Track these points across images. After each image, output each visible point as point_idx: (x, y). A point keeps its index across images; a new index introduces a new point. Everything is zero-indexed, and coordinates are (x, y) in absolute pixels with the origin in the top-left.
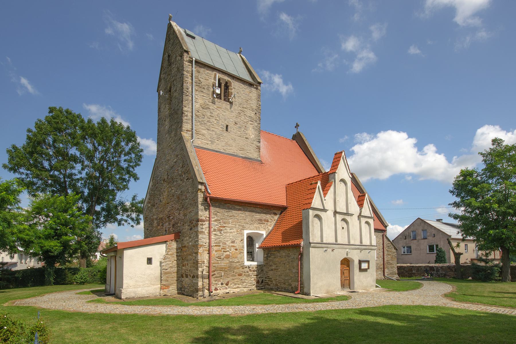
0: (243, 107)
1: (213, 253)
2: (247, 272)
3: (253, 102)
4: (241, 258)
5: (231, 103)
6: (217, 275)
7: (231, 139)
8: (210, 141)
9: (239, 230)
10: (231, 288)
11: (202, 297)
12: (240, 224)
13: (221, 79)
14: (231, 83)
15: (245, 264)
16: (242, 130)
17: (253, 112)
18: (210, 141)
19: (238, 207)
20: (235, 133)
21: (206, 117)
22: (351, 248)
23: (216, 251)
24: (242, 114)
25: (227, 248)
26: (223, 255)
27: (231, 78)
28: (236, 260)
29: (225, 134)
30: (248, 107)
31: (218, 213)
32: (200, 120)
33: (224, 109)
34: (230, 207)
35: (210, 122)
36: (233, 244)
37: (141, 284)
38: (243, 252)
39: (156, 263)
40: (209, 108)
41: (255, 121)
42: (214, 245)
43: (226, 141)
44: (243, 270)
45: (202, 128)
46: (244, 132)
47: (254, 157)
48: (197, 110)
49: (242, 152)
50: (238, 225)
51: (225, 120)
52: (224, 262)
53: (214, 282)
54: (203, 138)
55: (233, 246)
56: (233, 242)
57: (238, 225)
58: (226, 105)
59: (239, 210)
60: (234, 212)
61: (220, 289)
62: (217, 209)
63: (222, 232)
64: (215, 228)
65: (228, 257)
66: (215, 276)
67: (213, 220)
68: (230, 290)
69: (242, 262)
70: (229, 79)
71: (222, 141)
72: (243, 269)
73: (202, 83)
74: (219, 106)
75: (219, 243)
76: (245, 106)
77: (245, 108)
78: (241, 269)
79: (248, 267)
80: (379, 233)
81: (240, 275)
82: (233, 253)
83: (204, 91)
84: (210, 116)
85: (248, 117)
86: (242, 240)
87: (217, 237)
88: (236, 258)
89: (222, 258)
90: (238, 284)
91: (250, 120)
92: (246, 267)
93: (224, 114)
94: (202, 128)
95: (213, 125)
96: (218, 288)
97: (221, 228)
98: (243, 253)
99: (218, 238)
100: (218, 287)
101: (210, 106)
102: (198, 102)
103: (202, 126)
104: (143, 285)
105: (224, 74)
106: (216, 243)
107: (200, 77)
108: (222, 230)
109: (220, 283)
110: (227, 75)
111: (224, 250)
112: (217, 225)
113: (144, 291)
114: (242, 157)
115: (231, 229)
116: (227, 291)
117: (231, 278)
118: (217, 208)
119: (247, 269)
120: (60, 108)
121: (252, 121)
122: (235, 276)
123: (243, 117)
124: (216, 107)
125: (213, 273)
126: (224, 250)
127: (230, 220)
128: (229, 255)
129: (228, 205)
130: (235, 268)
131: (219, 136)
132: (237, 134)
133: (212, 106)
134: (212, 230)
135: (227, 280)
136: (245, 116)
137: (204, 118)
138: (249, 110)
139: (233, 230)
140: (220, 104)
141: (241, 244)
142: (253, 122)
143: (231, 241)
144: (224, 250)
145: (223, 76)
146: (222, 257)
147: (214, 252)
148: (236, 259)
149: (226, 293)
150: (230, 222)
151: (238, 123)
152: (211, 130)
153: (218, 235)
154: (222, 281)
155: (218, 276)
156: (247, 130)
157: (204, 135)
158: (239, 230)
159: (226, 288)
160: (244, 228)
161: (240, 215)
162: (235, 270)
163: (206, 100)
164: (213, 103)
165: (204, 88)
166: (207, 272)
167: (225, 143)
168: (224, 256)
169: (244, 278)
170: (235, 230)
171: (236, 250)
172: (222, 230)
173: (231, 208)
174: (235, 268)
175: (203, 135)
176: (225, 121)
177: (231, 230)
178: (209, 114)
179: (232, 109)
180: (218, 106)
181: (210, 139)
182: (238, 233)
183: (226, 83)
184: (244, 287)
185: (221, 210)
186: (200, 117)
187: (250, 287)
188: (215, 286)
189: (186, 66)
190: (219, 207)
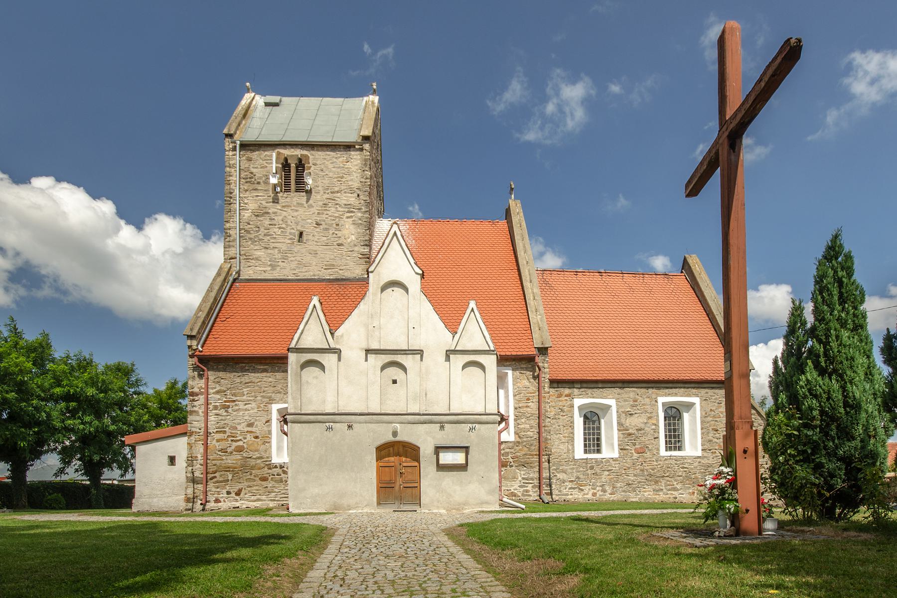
0: (331, 193)
1: (213, 443)
2: (277, 475)
3: (352, 178)
4: (266, 451)
5: (309, 192)
6: (219, 479)
7: (308, 254)
8: (270, 265)
9: (262, 405)
10: (245, 500)
11: (190, 512)
12: (264, 394)
13: (288, 158)
14: (307, 157)
15: (273, 462)
16: (331, 232)
17: (352, 195)
18: (270, 265)
19: (262, 367)
20: (316, 242)
21: (262, 229)
22: (406, 421)
23: (218, 441)
24: (330, 205)
25: (237, 435)
26: (230, 447)
27: (308, 148)
28: (257, 455)
29: (297, 248)
30: (343, 188)
31: (222, 380)
32: (252, 236)
33: (294, 206)
34: (247, 368)
35: (269, 235)
36: (250, 429)
37: (159, 493)
38: (268, 441)
39: (181, 462)
40: (268, 213)
41: (358, 209)
42: (215, 431)
43: (299, 259)
44: (270, 471)
45: (256, 248)
46: (334, 235)
47: (355, 275)
48: (246, 222)
49: (330, 270)
50: (262, 396)
51: (297, 224)
52: (234, 457)
53: (214, 489)
54: (257, 264)
55: (251, 432)
56: (250, 425)
57: (262, 396)
58: (302, 197)
59: (265, 371)
60: (253, 377)
61: (224, 501)
62: (221, 374)
63: (230, 410)
64: (216, 404)
65: (240, 449)
66: (215, 480)
67: (211, 391)
68: (242, 504)
69: (268, 457)
70: (305, 152)
71: (291, 261)
72: (270, 469)
73: (255, 175)
74: (287, 204)
75: (223, 428)
76: (336, 189)
77: (338, 192)
78: (266, 469)
79: (281, 466)
80: (717, 391)
81: (264, 479)
82: (250, 442)
83: (259, 188)
84: (270, 225)
85: (342, 207)
86: (267, 422)
87: (220, 418)
88: (257, 450)
89: (229, 451)
90: (260, 495)
91: (346, 210)
92: (276, 467)
93: (296, 214)
94: (255, 248)
95: (275, 238)
96: (222, 500)
97: (228, 404)
98: (269, 442)
99: (222, 420)
100: (222, 497)
101: (269, 209)
102: (249, 208)
103: (255, 245)
104: (162, 495)
105: (294, 147)
106: (219, 428)
107: (253, 168)
108: (228, 407)
109: (224, 491)
110: (300, 147)
111: (233, 438)
112: (219, 399)
113: (161, 503)
114: (329, 279)
115: (246, 404)
116: (237, 504)
117: (246, 484)
118: (221, 373)
119: (278, 470)
120: (850, 252)
121: (352, 212)
122: (255, 481)
123: (333, 209)
124: (280, 208)
125: (213, 475)
126: (233, 438)
127: (245, 390)
128: (243, 447)
129: (241, 365)
130: (253, 468)
131: (286, 253)
132: (320, 242)
133: (272, 208)
134: (211, 407)
135: (237, 487)
136: (337, 206)
137: (258, 231)
138: (345, 192)
139: (250, 405)
140: (288, 200)
141: (266, 429)
142: (354, 212)
143: (246, 423)
144: (233, 438)
145: (293, 150)
146: (229, 450)
147: (214, 442)
148: (256, 453)
149: (234, 508)
150: (245, 393)
151: (323, 223)
152: (271, 247)
153: (222, 416)
154: (228, 488)
155: (221, 479)
156: (340, 231)
157: (260, 259)
158: (262, 405)
159: (236, 501)
160: (271, 401)
161: (265, 379)
162: (253, 472)
163: (262, 202)
164: (276, 201)
165: (259, 183)
166: (202, 474)
167: (297, 262)
168: (233, 448)
169: (269, 484)
170: (254, 405)
171: (257, 437)
172: (228, 407)
173: (249, 370)
174: (253, 468)
175: (257, 259)
176: (298, 225)
177: (247, 406)
178: (267, 222)
179: (311, 202)
180: (284, 204)
181: (269, 263)
182: (260, 409)
183: (300, 160)
184: (271, 500)
185: (228, 375)
186: (252, 232)
187: (283, 501)
188: (216, 496)
189: (229, 158)
190: (225, 370)
